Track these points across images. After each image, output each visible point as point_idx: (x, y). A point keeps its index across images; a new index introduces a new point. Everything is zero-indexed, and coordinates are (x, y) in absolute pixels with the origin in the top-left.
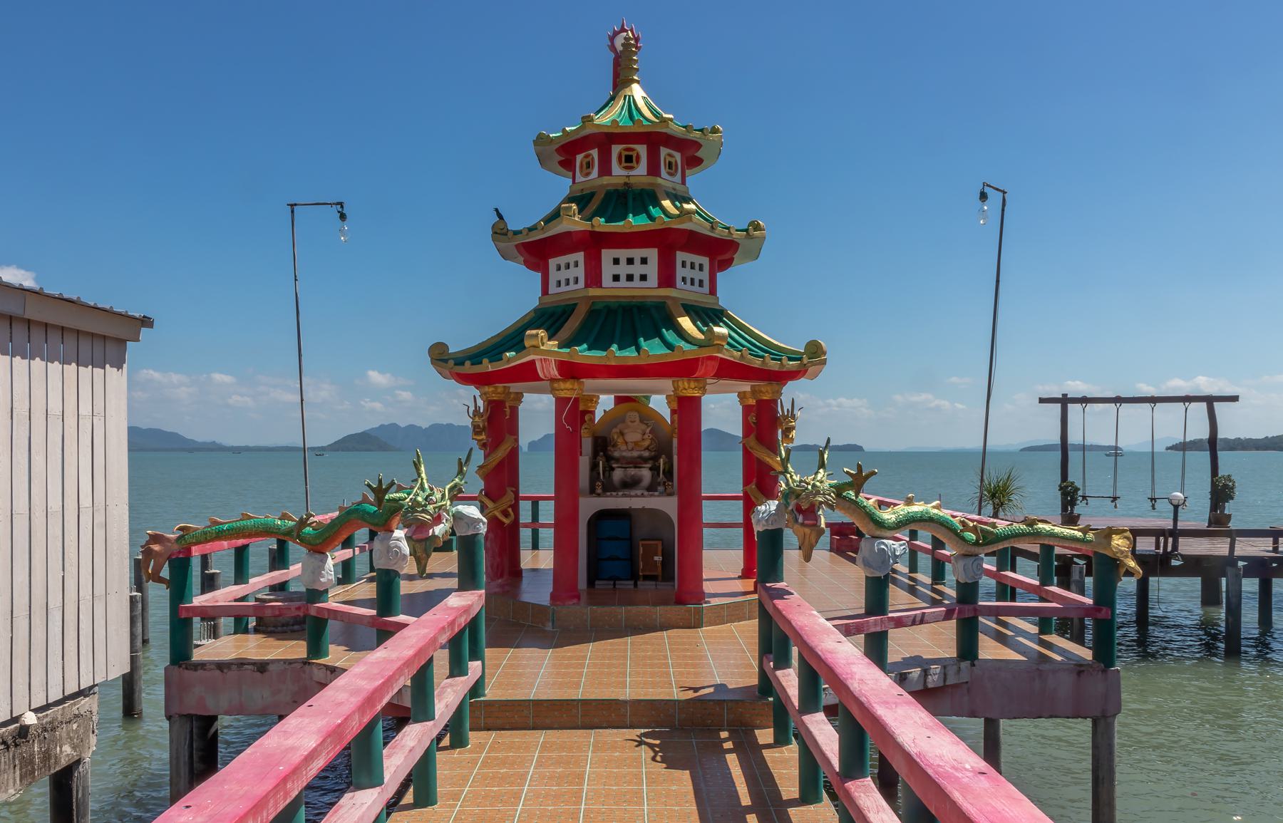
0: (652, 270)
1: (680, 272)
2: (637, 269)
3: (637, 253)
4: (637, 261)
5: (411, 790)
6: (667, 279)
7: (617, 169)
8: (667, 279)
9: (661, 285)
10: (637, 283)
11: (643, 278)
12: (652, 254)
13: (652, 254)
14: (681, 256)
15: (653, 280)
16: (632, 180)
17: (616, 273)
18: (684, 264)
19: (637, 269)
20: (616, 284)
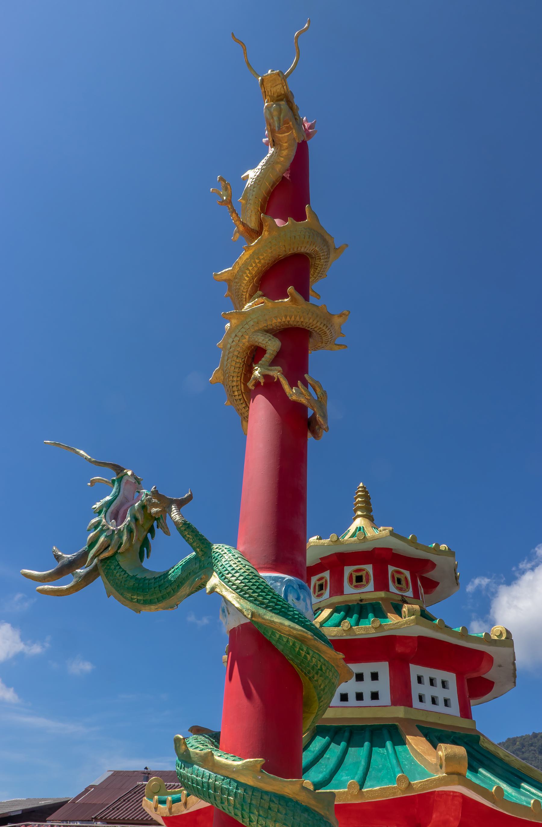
0: (383, 686)
1: (416, 689)
2: (367, 687)
3: (366, 668)
4: (367, 677)
5: (236, 664)
6: (402, 694)
7: (348, 588)
8: (402, 694)
9: (395, 702)
10: (441, 708)
11: (375, 696)
12: (383, 668)
13: (383, 668)
14: (415, 670)
15: (385, 697)
16: (363, 596)
17: (374, 690)
18: (420, 680)
19: (367, 687)
20: (360, 703)
